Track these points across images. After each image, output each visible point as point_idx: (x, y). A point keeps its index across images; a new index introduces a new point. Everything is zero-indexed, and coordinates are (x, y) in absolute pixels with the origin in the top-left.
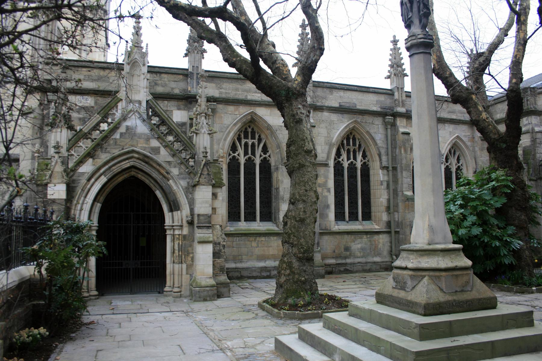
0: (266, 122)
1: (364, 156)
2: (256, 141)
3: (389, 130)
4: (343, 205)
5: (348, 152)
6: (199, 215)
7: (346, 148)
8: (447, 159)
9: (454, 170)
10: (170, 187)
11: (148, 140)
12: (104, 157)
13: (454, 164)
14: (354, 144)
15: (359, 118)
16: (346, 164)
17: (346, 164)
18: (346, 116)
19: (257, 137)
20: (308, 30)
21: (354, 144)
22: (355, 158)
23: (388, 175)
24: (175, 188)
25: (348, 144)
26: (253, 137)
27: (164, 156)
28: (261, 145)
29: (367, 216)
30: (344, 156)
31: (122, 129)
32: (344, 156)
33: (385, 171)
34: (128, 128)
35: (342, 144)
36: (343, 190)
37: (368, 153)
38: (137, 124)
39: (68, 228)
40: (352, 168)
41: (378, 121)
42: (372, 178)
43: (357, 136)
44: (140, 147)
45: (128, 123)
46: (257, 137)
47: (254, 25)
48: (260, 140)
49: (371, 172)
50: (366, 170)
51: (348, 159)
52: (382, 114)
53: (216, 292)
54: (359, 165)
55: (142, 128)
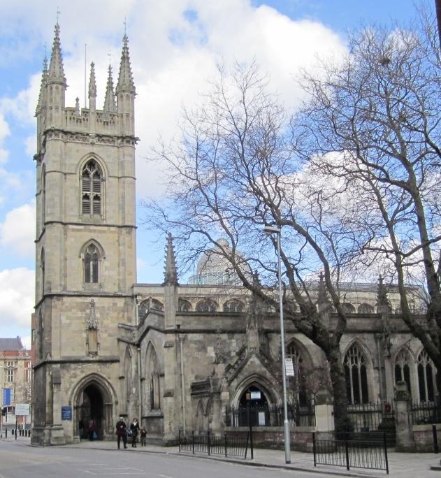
1: (362, 361)
2: (295, 355)
5: (352, 358)
8: (419, 359)
9: (425, 366)
12: (241, 377)
14: (356, 353)
15: (358, 336)
17: (351, 367)
18: (350, 335)
19: (295, 352)
20: (324, 280)
21: (356, 353)
22: (356, 362)
23: (379, 373)
24: (274, 391)
25: (352, 353)
26: (293, 353)
27: (268, 375)
28: (299, 357)
29: (366, 400)
30: (349, 361)
31: (249, 363)
32: (349, 361)
34: (252, 362)
36: (354, 387)
37: (365, 359)
38: (255, 360)
39: (388, 407)
40: (355, 369)
41: (371, 336)
42: (368, 375)
44: (258, 370)
45: (251, 360)
46: (295, 352)
48: (297, 354)
49: (367, 371)
50: (364, 369)
51: (352, 363)
52: (373, 332)
54: (359, 365)
55: (257, 362)
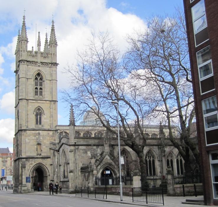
0: (127, 150)
1: (153, 157)
3: (160, 150)
4: (181, 166)
6: (30, 182)
7: (148, 155)
8: (177, 157)
9: (179, 160)
10: (115, 170)
11: (110, 160)
12: (102, 164)
13: (179, 158)
14: (150, 154)
15: (151, 147)
16: (148, 160)
17: (148, 160)
18: (148, 147)
19: (125, 154)
21: (150, 154)
22: (150, 158)
23: (160, 163)
25: (148, 154)
26: (124, 154)
28: (126, 156)
29: (154, 174)
30: (148, 158)
31: (105, 158)
32: (148, 158)
33: (159, 162)
35: (147, 154)
37: (154, 157)
38: (108, 157)
40: (150, 161)
41: (156, 147)
42: (155, 164)
43: (151, 152)
44: (109, 161)
45: (106, 157)
46: (125, 154)
47: (145, 197)
49: (155, 162)
50: (154, 161)
51: (149, 158)
53: (199, 115)
55: (109, 158)
